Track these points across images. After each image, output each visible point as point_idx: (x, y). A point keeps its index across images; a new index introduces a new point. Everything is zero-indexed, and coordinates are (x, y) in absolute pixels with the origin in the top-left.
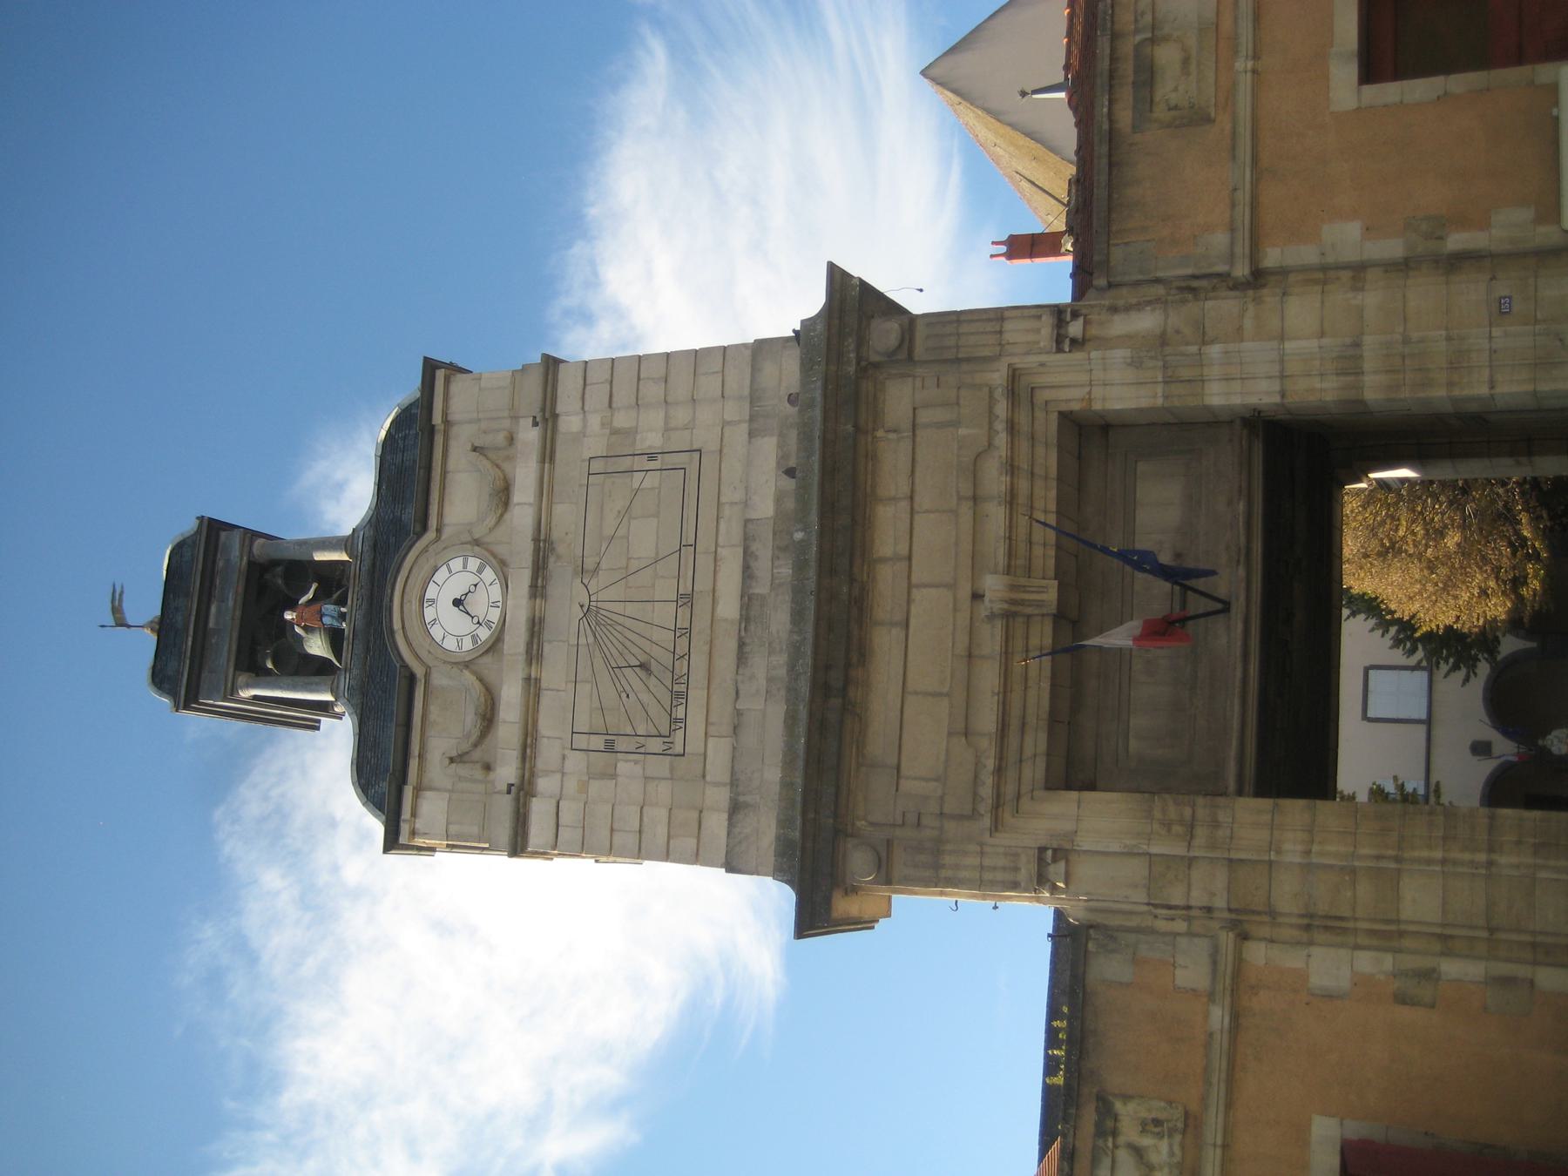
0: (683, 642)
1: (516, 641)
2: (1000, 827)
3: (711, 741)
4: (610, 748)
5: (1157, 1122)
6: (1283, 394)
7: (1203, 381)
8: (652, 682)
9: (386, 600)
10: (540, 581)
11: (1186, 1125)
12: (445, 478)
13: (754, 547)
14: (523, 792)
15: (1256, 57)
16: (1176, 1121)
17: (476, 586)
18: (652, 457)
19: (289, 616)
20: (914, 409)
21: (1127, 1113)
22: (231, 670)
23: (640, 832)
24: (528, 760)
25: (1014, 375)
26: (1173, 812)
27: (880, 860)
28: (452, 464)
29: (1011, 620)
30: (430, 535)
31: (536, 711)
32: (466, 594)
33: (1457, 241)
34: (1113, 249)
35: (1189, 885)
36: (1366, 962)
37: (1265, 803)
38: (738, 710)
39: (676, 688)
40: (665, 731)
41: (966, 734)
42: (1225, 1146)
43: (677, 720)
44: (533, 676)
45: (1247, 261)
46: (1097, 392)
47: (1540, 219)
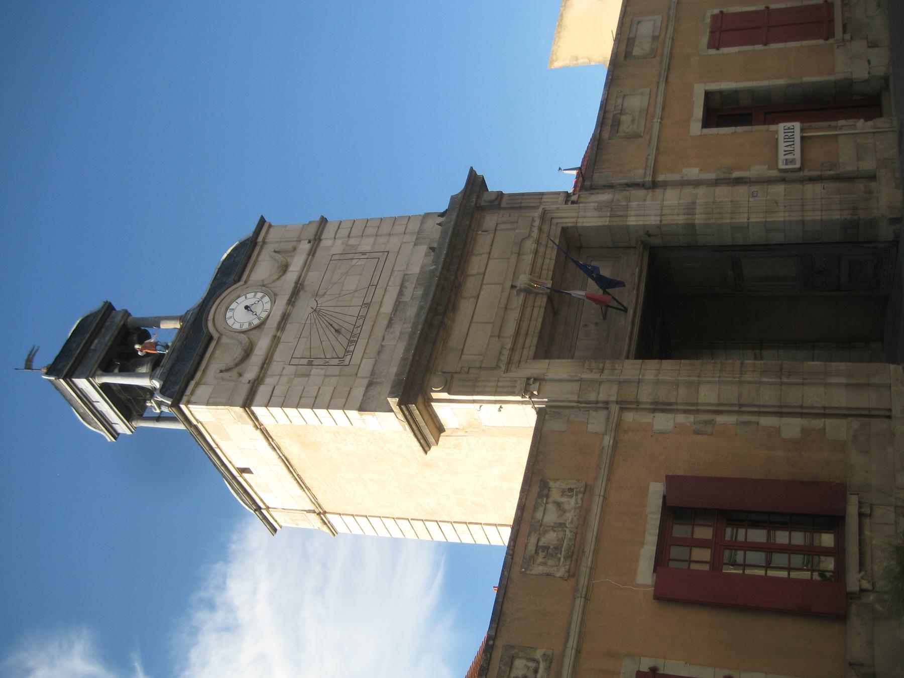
0: (360, 322)
1: (272, 323)
2: (509, 371)
3: (364, 361)
4: (310, 364)
5: (571, 490)
6: (661, 221)
7: (627, 216)
8: (340, 337)
9: (208, 307)
10: (293, 299)
11: (585, 490)
12: (255, 263)
13: (406, 284)
15: (661, 119)
16: (581, 488)
17: (256, 315)
18: (364, 254)
19: (137, 346)
20: (497, 224)
21: (555, 487)
22: (96, 366)
23: (316, 397)
24: (264, 369)
25: (545, 212)
26: (594, 365)
27: (447, 381)
28: (261, 258)
29: (528, 295)
30: (241, 283)
31: (274, 350)
32: (251, 311)
33: (736, 174)
34: (594, 174)
35: (599, 393)
36: (681, 418)
37: (639, 361)
38: (382, 345)
39: (352, 339)
40: (341, 355)
41: (499, 337)
42: (605, 498)
44: (278, 335)
45: (651, 176)
46: (579, 220)
47: (769, 168)
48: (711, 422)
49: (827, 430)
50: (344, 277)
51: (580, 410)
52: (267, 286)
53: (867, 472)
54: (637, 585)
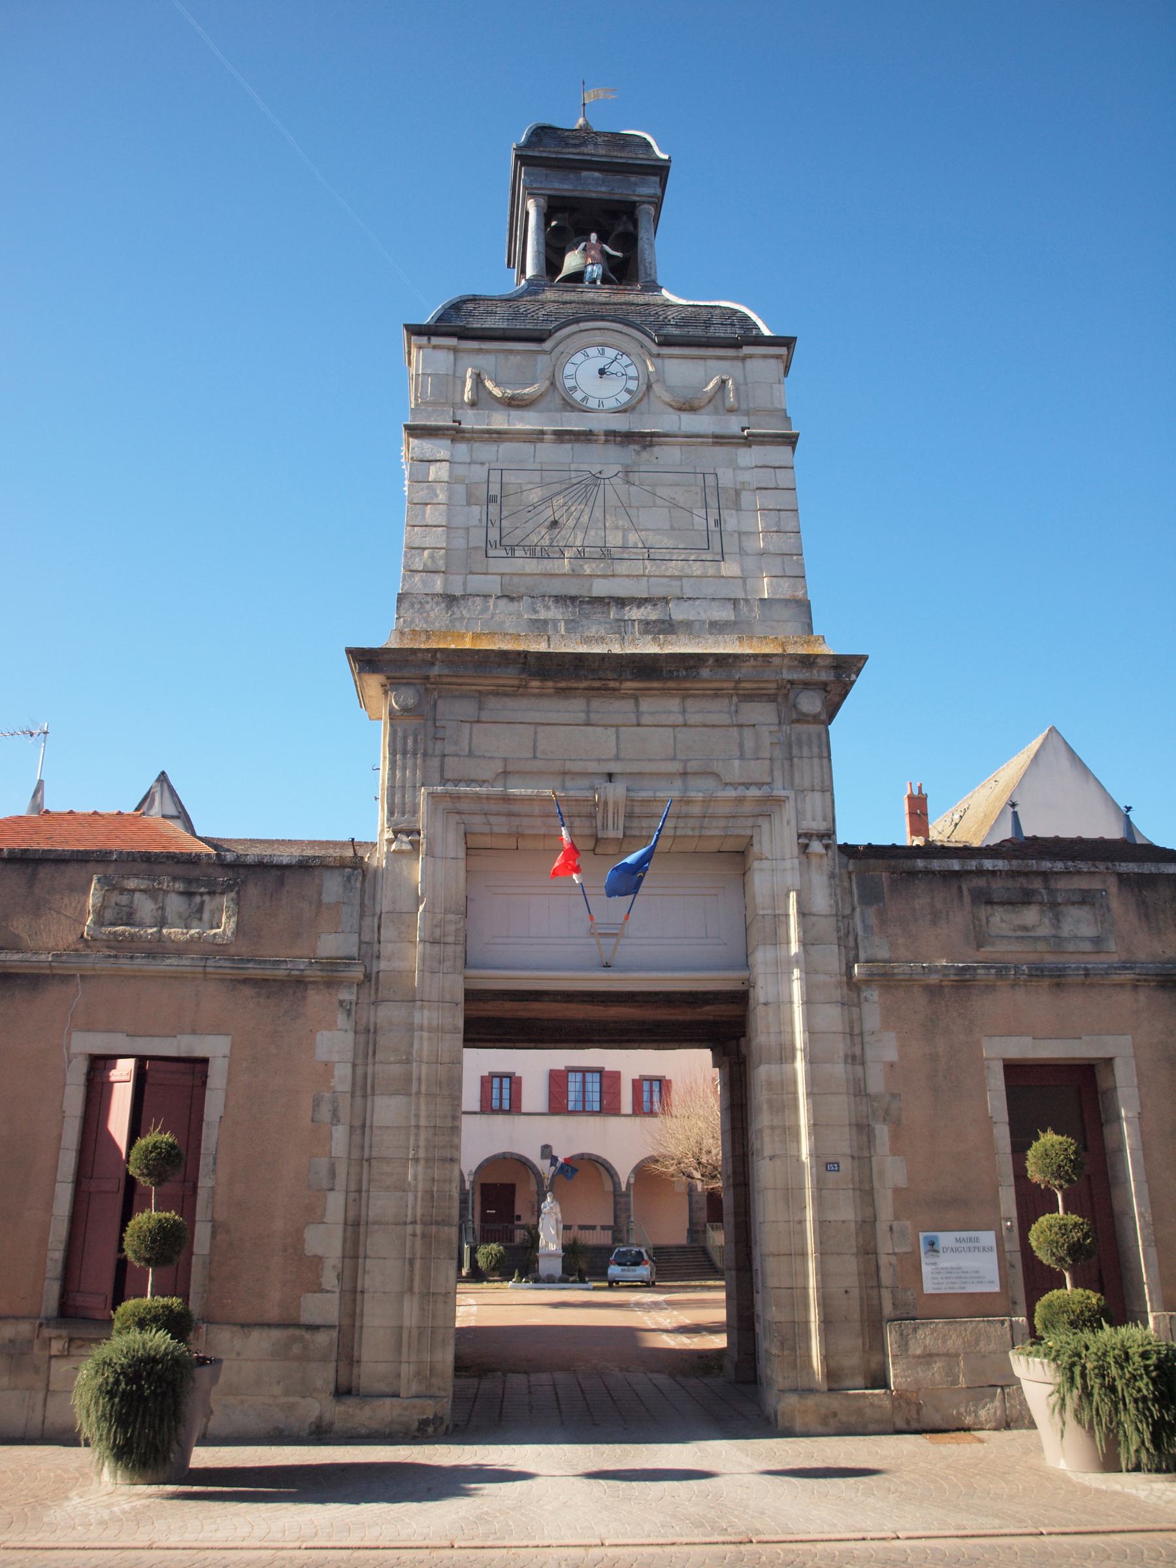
14: (456, 434)
18: (718, 523)
22: (548, 192)
40: (505, 541)
43: (513, 550)
44: (545, 437)
48: (335, 1117)
49: (318, 1295)
50: (668, 504)
51: (813, 925)
52: (719, 394)
53: (238, 1354)
54: (69, 1034)
